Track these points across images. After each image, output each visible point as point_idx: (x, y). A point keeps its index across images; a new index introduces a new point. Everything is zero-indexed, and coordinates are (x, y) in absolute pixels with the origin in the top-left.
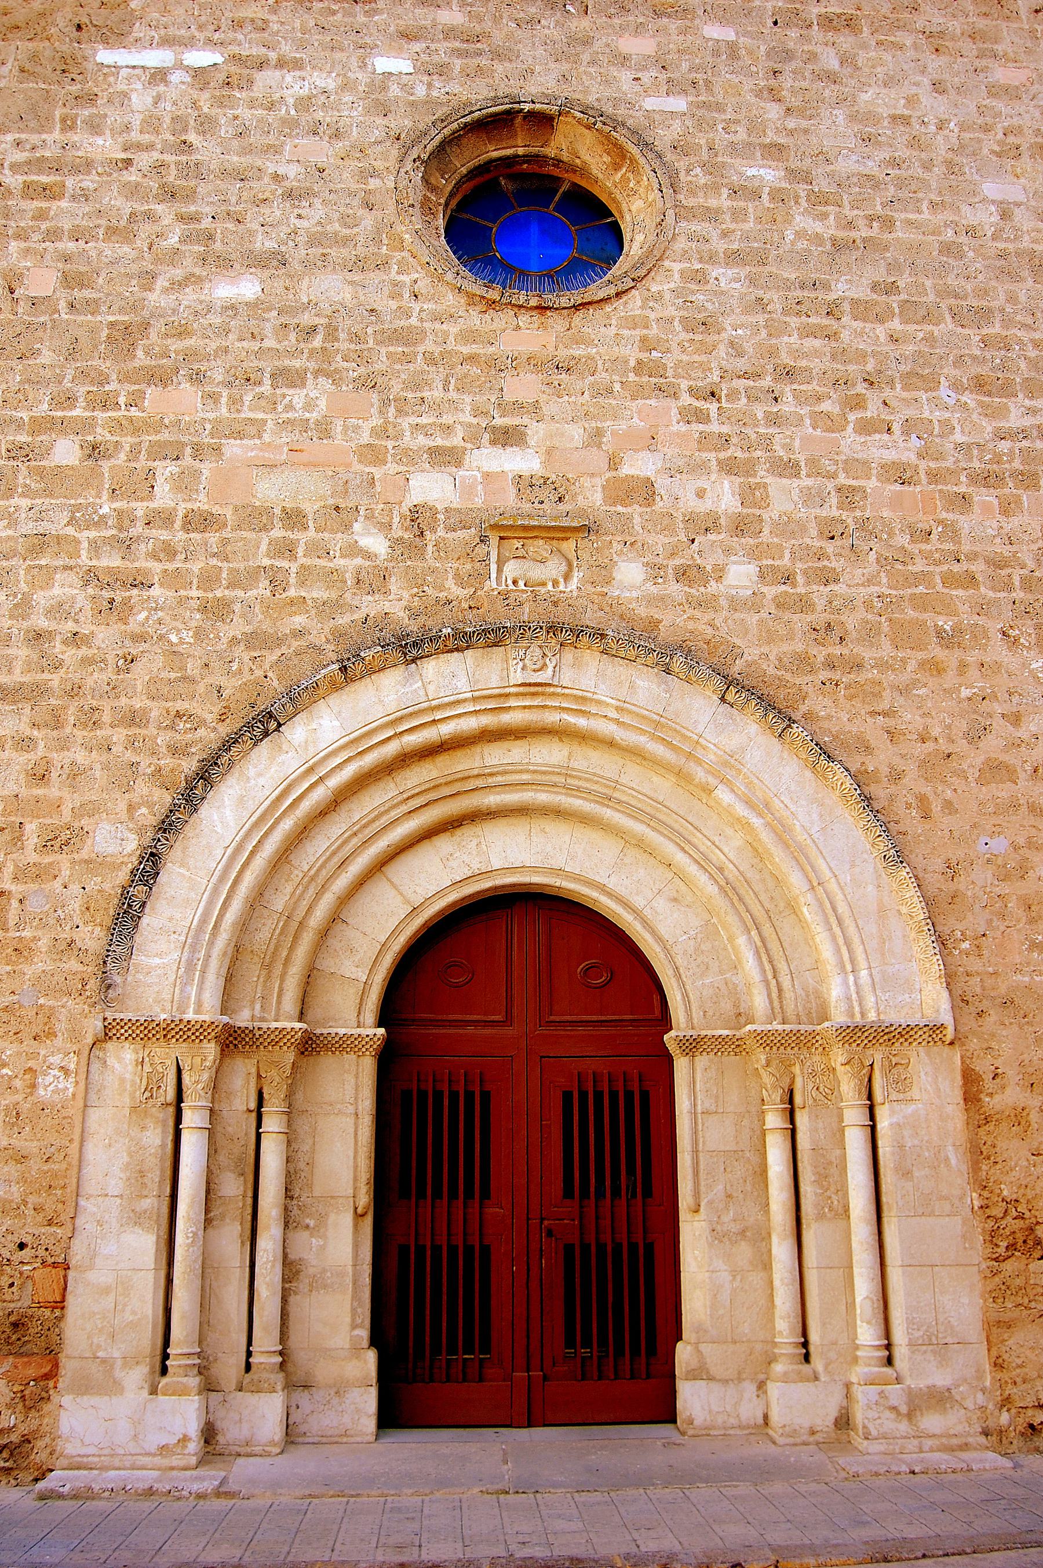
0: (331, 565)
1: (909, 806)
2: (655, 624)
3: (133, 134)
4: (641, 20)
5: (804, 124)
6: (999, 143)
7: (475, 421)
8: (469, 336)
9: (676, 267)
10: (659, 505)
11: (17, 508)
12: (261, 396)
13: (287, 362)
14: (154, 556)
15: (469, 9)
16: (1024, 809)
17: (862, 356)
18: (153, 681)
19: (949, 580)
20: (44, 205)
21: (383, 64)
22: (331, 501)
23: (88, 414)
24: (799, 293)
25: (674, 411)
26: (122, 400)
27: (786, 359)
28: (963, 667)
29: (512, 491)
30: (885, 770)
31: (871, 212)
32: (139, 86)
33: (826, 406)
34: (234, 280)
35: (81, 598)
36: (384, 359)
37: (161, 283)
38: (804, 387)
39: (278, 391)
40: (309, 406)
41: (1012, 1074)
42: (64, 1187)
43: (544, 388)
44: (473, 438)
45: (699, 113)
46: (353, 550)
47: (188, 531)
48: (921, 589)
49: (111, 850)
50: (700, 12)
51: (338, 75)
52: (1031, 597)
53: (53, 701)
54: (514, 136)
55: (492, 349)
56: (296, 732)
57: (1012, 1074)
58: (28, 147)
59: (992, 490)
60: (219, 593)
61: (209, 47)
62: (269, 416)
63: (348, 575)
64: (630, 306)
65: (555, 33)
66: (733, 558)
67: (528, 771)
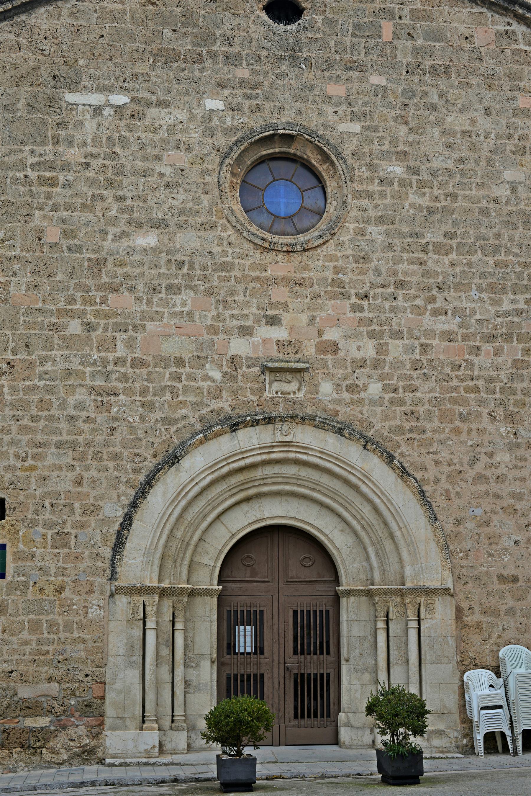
0: (197, 385)
1: (441, 495)
2: (336, 412)
3: (88, 147)
4: (339, 72)
5: (418, 138)
6: (516, 146)
7: (258, 312)
8: (254, 267)
9: (352, 226)
10: (341, 354)
11: (55, 356)
12: (160, 299)
13: (172, 281)
14: (119, 380)
15: (251, 67)
16: (491, 495)
17: (437, 274)
18: (123, 439)
19: (467, 389)
20: (49, 189)
21: (211, 104)
22: (195, 354)
23: (83, 308)
24: (409, 240)
25: (348, 306)
26: (98, 300)
27: (401, 277)
28: (470, 431)
29: (276, 348)
30: (432, 479)
31: (447, 191)
32: (88, 117)
33: (418, 302)
34: (145, 235)
35: (89, 400)
36: (216, 279)
37: (110, 237)
38: (408, 292)
39: (169, 297)
40: (183, 304)
41: (477, 608)
42: (102, 653)
43: (289, 294)
44: (257, 321)
45: (366, 133)
46: (206, 378)
47: (133, 368)
48: (454, 394)
49: (111, 515)
50: (369, 66)
51: (187, 111)
52: (503, 397)
53: (81, 449)
54: (275, 142)
55: (265, 274)
56: (186, 463)
57: (477, 608)
58: (37, 154)
59: (491, 344)
60: (149, 398)
61: (121, 93)
62: (166, 310)
63: (205, 390)
64: (329, 249)
65: (294, 83)
66: (372, 380)
67: (281, 477)
